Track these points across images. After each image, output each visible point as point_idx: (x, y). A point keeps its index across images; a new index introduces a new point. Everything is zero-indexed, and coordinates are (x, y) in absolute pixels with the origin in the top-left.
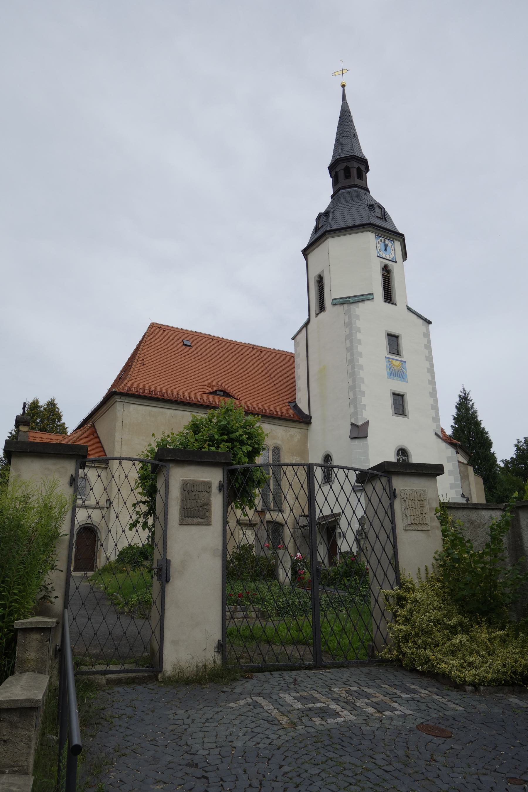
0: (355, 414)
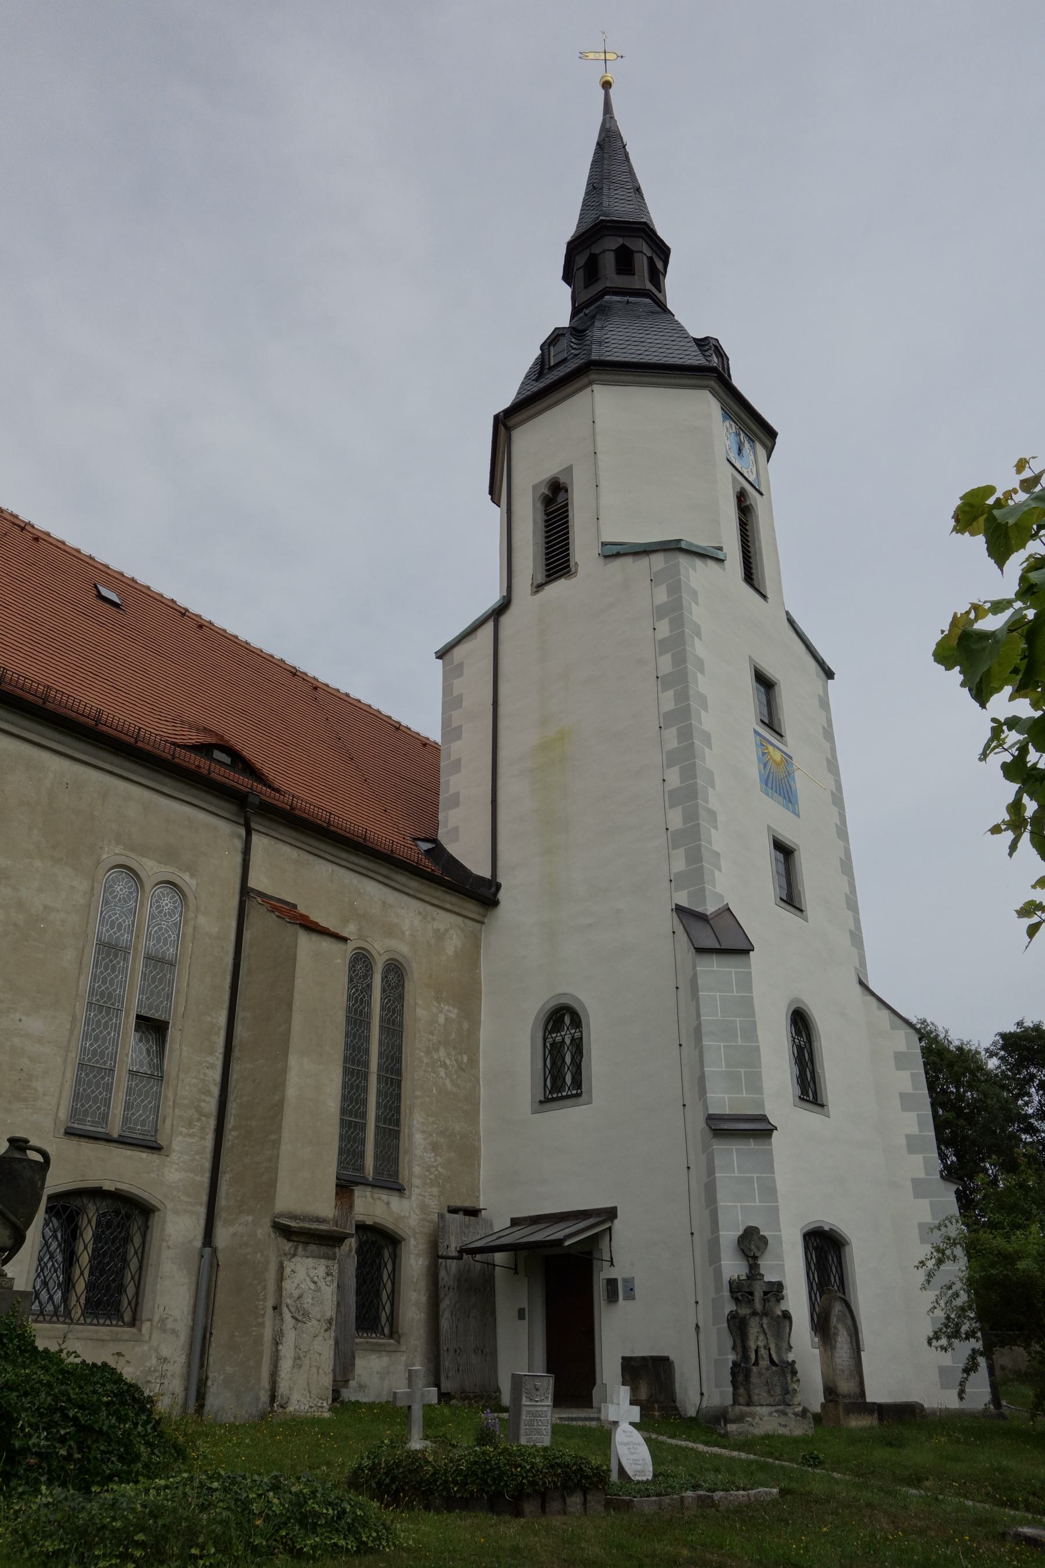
0: (695, 875)
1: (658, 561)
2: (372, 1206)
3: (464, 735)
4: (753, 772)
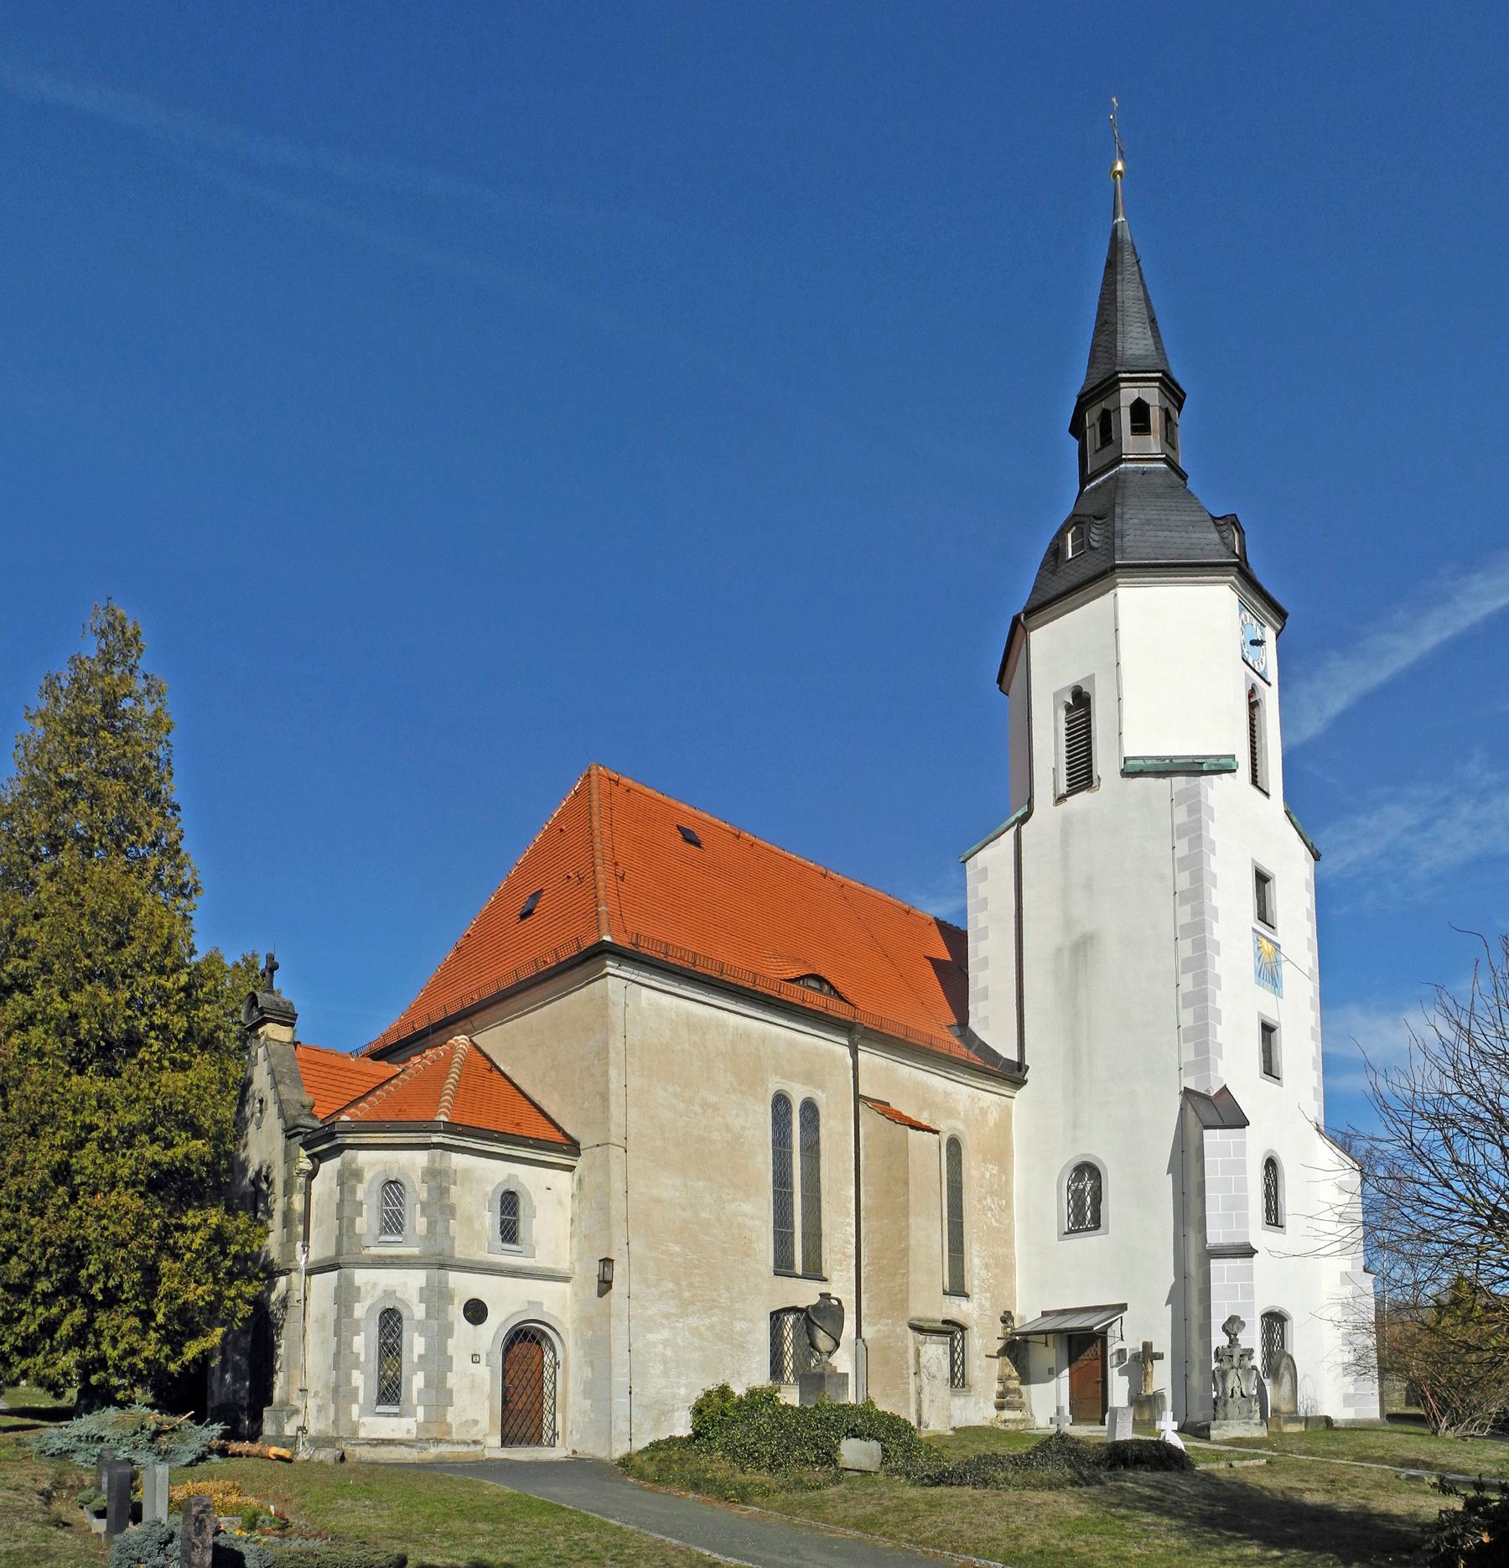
1: (1180, 782)
2: (957, 1309)
3: (990, 934)
4: (1250, 967)
